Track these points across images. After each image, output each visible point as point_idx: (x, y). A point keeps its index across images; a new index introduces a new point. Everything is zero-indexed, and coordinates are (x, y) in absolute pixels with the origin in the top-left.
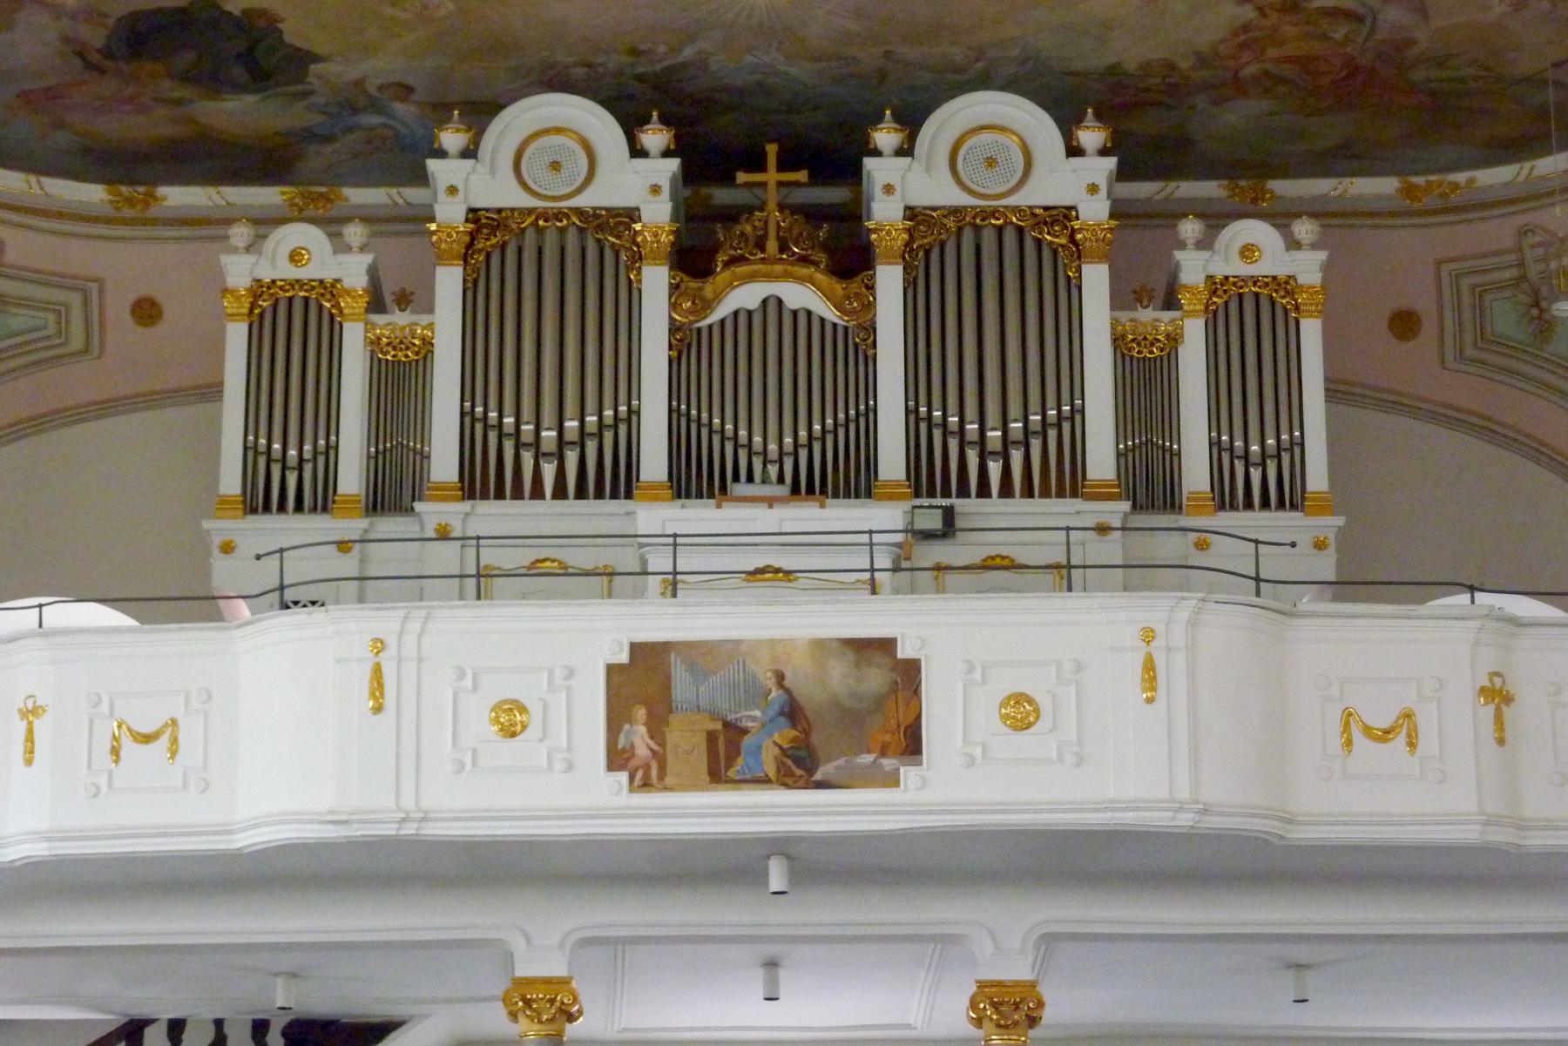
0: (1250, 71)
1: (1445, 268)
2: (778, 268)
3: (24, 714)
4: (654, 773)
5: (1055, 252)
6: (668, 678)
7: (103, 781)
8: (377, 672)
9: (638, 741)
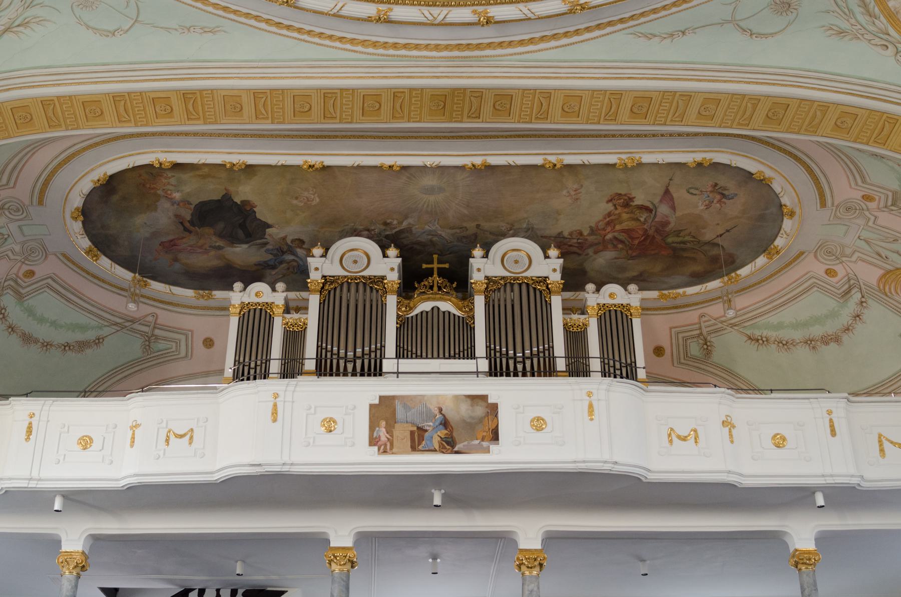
0: (609, 236)
1: (673, 330)
2: (438, 296)
3: (131, 428)
4: (388, 447)
5: (541, 292)
6: (395, 410)
7: (161, 453)
8: (275, 405)
9: (381, 434)
